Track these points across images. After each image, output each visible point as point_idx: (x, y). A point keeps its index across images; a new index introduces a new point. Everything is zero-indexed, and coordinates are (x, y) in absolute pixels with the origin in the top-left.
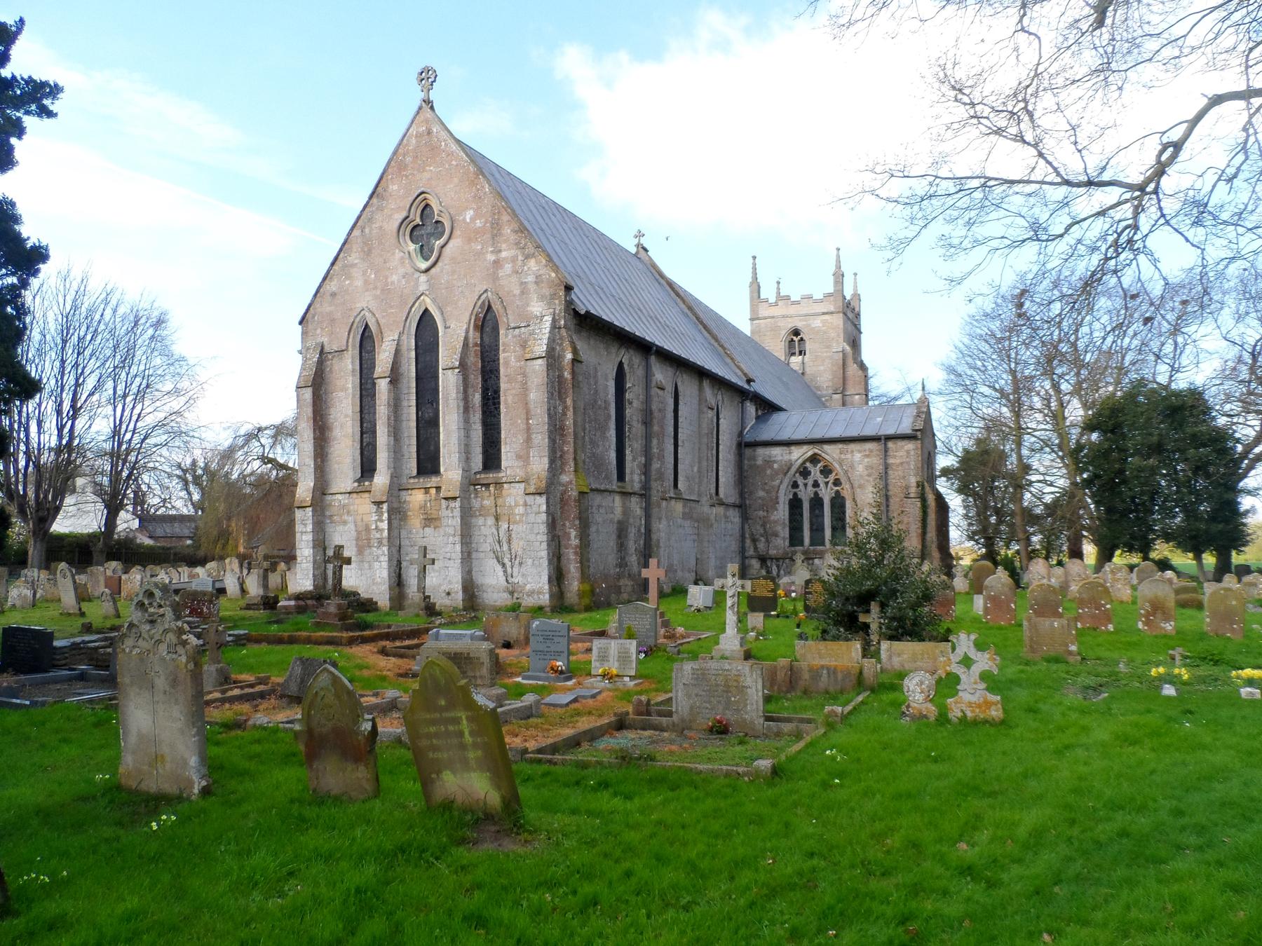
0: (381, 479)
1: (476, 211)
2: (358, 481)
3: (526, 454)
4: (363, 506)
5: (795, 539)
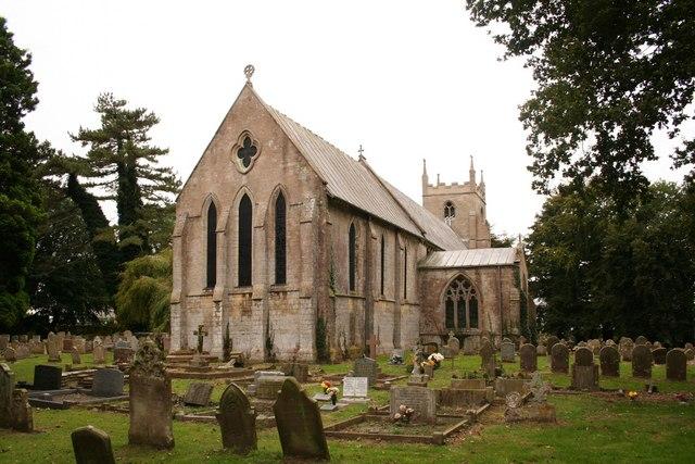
0: (218, 289)
1: (275, 141)
2: (206, 289)
3: (301, 277)
4: (208, 303)
5: (449, 325)
